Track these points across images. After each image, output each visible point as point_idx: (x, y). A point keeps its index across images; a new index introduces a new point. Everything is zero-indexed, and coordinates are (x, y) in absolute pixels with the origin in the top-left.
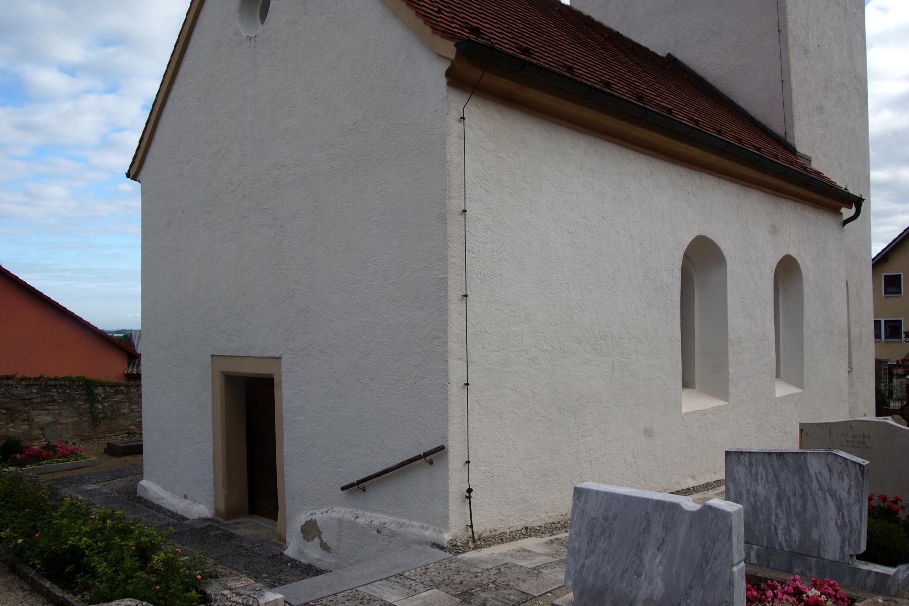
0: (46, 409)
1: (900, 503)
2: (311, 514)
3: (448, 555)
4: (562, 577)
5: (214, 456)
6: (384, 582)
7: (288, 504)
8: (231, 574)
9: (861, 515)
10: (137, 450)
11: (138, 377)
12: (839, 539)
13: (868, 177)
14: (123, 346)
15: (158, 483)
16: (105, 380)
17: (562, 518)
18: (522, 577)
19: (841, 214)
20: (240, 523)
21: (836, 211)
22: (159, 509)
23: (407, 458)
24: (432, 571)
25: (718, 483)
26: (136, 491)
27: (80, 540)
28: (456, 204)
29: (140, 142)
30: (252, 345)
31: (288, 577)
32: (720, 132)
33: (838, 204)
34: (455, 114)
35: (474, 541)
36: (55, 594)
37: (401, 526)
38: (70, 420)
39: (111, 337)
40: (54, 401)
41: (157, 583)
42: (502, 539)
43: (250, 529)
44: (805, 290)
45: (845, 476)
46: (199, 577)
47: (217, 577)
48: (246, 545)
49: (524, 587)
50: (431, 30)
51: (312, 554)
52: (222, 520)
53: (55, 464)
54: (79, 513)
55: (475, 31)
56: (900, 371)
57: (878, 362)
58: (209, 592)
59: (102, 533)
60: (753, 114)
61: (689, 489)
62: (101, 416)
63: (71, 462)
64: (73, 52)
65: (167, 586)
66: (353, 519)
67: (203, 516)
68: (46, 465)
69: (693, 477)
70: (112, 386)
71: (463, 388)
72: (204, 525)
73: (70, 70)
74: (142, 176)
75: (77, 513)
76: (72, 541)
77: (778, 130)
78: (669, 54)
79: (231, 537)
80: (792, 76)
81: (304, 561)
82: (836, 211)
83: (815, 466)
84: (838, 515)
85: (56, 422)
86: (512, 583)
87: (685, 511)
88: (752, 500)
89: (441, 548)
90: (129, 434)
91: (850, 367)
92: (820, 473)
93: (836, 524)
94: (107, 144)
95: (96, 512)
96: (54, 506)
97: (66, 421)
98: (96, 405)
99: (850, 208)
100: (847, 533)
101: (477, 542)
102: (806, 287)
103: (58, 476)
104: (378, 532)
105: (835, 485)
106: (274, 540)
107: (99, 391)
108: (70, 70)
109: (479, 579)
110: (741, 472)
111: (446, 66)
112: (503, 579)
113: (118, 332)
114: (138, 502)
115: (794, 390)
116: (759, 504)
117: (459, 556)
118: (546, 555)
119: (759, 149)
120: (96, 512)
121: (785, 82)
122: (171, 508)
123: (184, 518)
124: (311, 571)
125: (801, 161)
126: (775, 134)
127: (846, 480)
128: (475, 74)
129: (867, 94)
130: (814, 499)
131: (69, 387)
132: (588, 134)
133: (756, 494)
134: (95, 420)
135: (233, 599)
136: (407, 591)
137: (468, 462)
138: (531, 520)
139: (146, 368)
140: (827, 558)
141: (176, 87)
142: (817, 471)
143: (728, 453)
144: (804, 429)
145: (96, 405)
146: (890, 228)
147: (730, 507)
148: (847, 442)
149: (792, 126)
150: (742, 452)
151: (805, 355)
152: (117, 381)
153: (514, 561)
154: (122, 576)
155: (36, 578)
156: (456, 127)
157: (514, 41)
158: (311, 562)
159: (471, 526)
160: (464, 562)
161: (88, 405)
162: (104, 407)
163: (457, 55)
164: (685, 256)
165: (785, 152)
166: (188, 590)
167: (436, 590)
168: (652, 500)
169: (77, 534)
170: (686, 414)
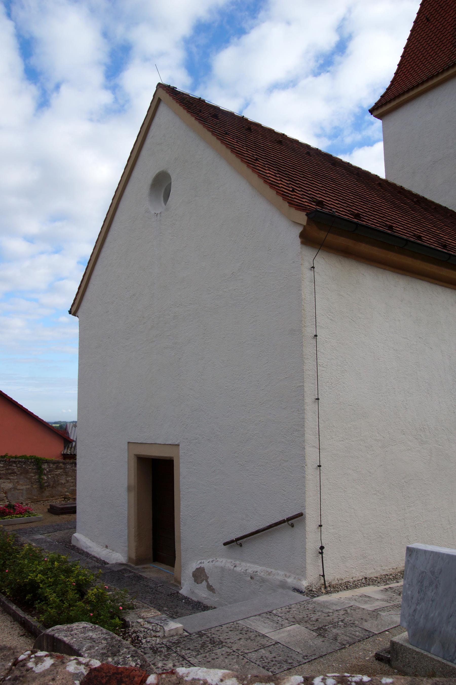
0: (9, 479)
2: (201, 563)
3: (305, 598)
4: (397, 619)
5: (128, 517)
6: (257, 617)
7: (183, 553)
8: (143, 606)
10: (73, 510)
11: (73, 457)
14: (60, 434)
15: (86, 535)
16: (49, 458)
17: (393, 571)
18: (365, 617)
20: (146, 568)
22: (87, 555)
23: (274, 522)
24: (294, 610)
26: (70, 541)
27: (37, 576)
28: (309, 331)
29: (79, 289)
30: (156, 436)
31: (183, 611)
34: (307, 265)
35: (326, 588)
36: (19, 615)
37: (269, 574)
38: (24, 487)
39: (53, 427)
40: (14, 473)
41: (92, 611)
42: (347, 586)
43: (154, 572)
46: (121, 608)
47: (133, 608)
48: (151, 585)
49: (367, 626)
50: (288, 204)
51: (200, 593)
52: (133, 565)
53: (14, 518)
54: (33, 556)
55: (320, 203)
58: (128, 619)
59: (51, 571)
62: (46, 484)
63: (25, 517)
64: (33, 226)
65: (98, 614)
66: (232, 567)
67: (119, 561)
68: (8, 519)
70: (54, 463)
71: (316, 469)
72: (120, 569)
73: (30, 239)
74: (80, 313)
75: (33, 556)
76: (31, 576)
79: (140, 578)
81: (195, 599)
85: (15, 488)
86: (357, 622)
89: (301, 592)
90: (65, 498)
94: (52, 289)
95: (48, 555)
96: (16, 550)
97: (22, 488)
98: (42, 477)
101: (328, 588)
103: (17, 527)
104: (252, 578)
106: (172, 582)
107: (45, 466)
108: (30, 239)
109: (330, 618)
111: (300, 229)
112: (350, 618)
113: (55, 423)
114: (72, 549)
117: (315, 599)
118: (383, 600)
120: (48, 555)
122: (96, 555)
123: (105, 563)
124: (199, 607)
128: (322, 235)
131: (25, 463)
132: (406, 275)
134: (42, 488)
135: (145, 626)
136: (275, 625)
137: (321, 526)
138: (370, 572)
139: (80, 452)
141: (104, 250)
145: (42, 477)
152: (57, 459)
153: (357, 604)
154: (66, 605)
155: (6, 602)
156: (308, 274)
157: (348, 209)
158: (200, 600)
159: (323, 576)
160: (319, 604)
161: (37, 477)
162: (48, 478)
166: (112, 618)
167: (297, 625)
169: (34, 571)
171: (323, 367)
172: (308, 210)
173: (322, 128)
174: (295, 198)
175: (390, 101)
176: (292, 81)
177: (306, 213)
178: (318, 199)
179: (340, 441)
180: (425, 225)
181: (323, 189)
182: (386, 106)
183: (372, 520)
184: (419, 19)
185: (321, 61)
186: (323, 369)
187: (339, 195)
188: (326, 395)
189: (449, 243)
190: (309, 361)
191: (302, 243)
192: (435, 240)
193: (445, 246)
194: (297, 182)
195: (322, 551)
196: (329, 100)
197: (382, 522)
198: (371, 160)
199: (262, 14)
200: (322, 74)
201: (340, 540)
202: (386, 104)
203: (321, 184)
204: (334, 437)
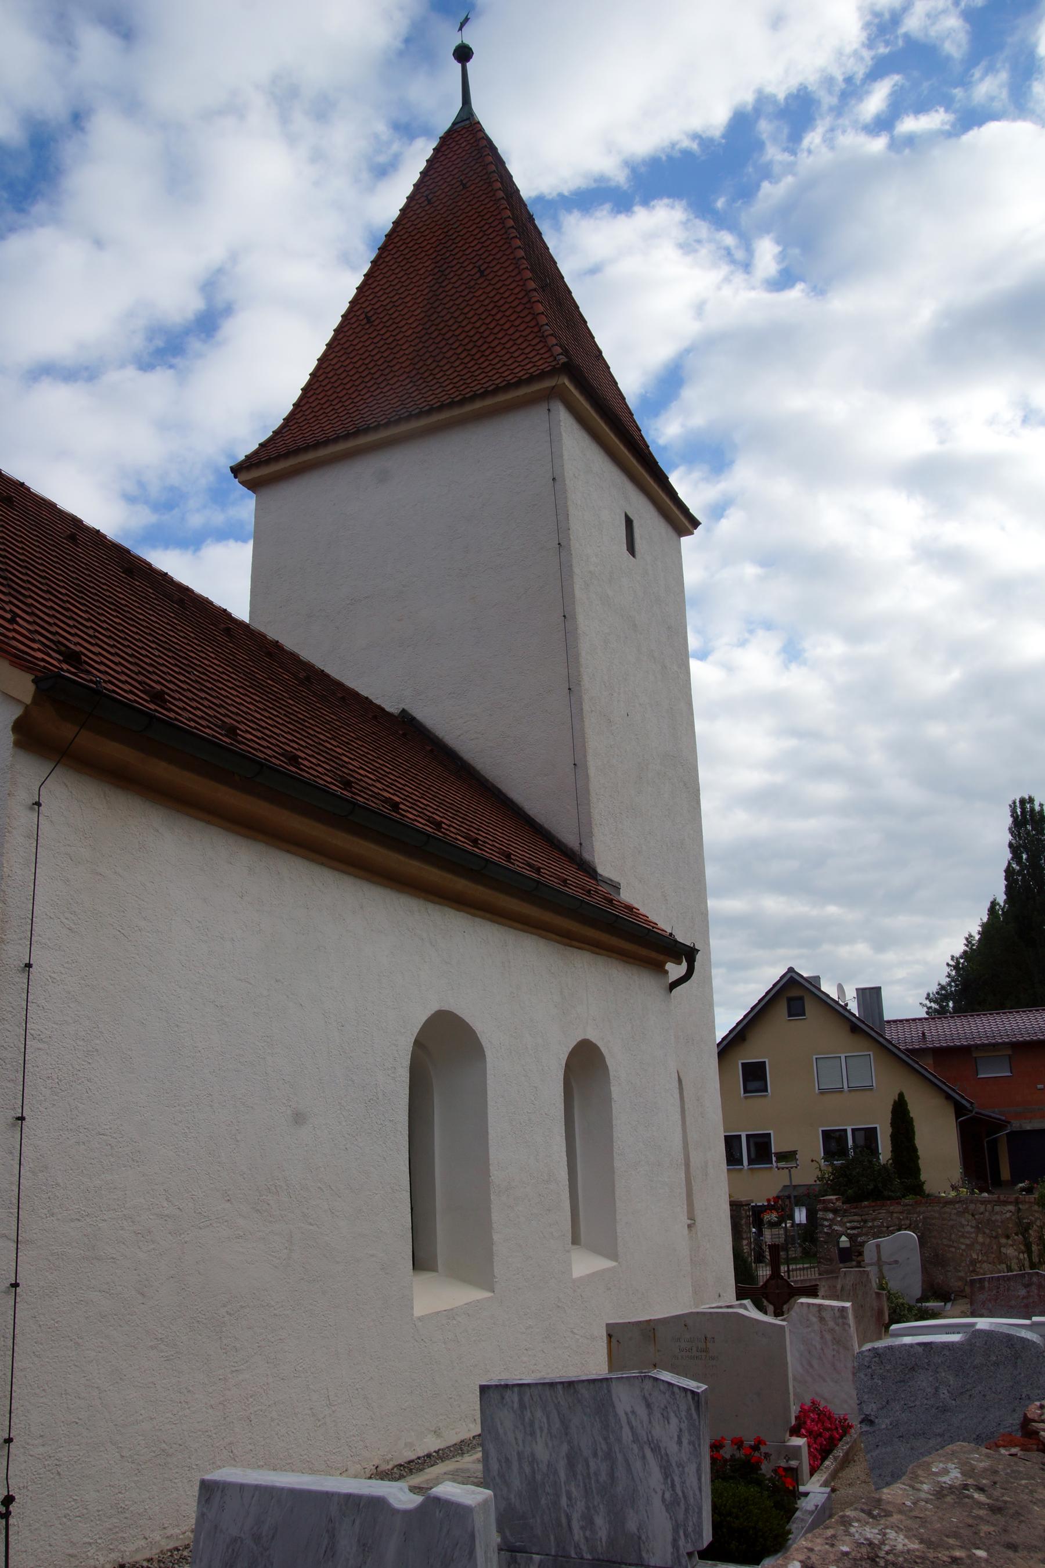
1: (763, 1449)
9: (699, 1479)
12: (669, 1526)
13: (704, 914)
19: (667, 972)
21: (659, 969)
25: (460, 1448)
32: (475, 842)
33: (661, 957)
44: (615, 1095)
45: (672, 1415)
55: (73, 658)
56: (773, 1216)
57: (735, 1206)
60: (531, 813)
61: (429, 1456)
69: (437, 1433)
77: (570, 839)
78: (404, 710)
80: (590, 758)
82: (659, 969)
83: (625, 1400)
84: (665, 1483)
87: (395, 1512)
88: (527, 1470)
91: (691, 1216)
92: (633, 1412)
93: (663, 1500)
99: (680, 963)
100: (681, 1516)
102: (615, 1090)
105: (657, 1431)
110: (506, 1420)
111: (17, 712)
115: (602, 1264)
116: (539, 1477)
119: (538, 870)
121: (578, 766)
125: (604, 888)
126: (565, 846)
127: (674, 1420)
128: (67, 731)
129: (699, 790)
130: (627, 1461)
132: (255, 839)
133: (533, 1460)
140: (652, 1563)
142: (629, 1410)
143: (484, 1389)
144: (614, 1334)
146: (752, 986)
147: (468, 1495)
148: (681, 1350)
149: (590, 835)
150: (506, 1386)
151: (618, 1203)
156: (24, 819)
157: (141, 678)
163: (34, 698)
164: (418, 1043)
165: (580, 875)
168: (339, 1494)
170: (420, 1319)
171: (41, 1041)
172: (40, 671)
173: (141, 484)
174: (14, 638)
175: (278, 458)
176: (87, 368)
177: (33, 677)
178: (72, 647)
179: (72, 1220)
180: (312, 732)
181: (88, 624)
182: (270, 465)
183: (143, 1412)
184: (353, 314)
185: (160, 343)
186: (41, 1046)
187: (126, 643)
188: (42, 1109)
189: (359, 777)
190: (7, 1026)
191: (18, 744)
192: (328, 767)
193: (347, 785)
194: (30, 601)
195: (7, 1508)
196: (164, 426)
197: (169, 1415)
198: (223, 576)
199: (40, 208)
200: (158, 368)
201: (59, 1474)
202: (268, 462)
203: (86, 612)
204: (56, 1210)
